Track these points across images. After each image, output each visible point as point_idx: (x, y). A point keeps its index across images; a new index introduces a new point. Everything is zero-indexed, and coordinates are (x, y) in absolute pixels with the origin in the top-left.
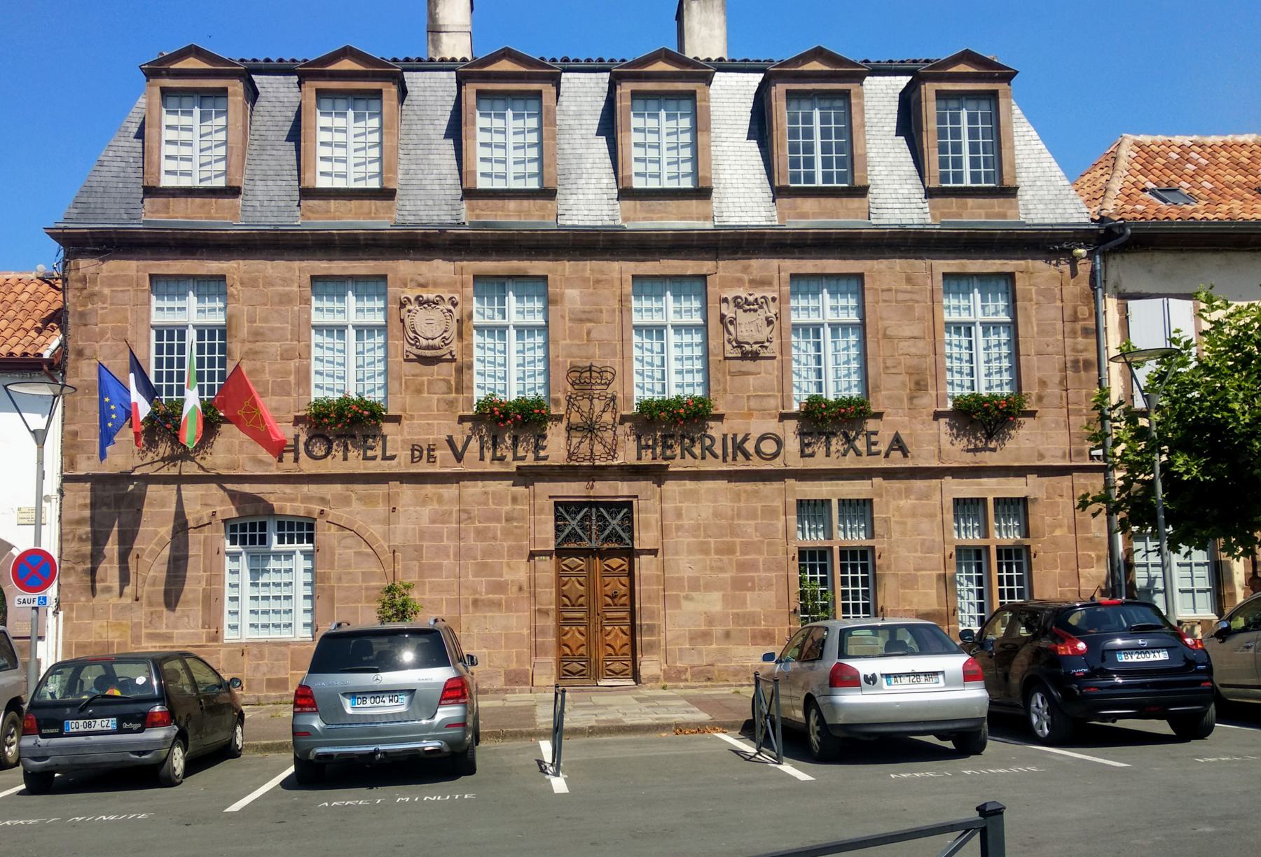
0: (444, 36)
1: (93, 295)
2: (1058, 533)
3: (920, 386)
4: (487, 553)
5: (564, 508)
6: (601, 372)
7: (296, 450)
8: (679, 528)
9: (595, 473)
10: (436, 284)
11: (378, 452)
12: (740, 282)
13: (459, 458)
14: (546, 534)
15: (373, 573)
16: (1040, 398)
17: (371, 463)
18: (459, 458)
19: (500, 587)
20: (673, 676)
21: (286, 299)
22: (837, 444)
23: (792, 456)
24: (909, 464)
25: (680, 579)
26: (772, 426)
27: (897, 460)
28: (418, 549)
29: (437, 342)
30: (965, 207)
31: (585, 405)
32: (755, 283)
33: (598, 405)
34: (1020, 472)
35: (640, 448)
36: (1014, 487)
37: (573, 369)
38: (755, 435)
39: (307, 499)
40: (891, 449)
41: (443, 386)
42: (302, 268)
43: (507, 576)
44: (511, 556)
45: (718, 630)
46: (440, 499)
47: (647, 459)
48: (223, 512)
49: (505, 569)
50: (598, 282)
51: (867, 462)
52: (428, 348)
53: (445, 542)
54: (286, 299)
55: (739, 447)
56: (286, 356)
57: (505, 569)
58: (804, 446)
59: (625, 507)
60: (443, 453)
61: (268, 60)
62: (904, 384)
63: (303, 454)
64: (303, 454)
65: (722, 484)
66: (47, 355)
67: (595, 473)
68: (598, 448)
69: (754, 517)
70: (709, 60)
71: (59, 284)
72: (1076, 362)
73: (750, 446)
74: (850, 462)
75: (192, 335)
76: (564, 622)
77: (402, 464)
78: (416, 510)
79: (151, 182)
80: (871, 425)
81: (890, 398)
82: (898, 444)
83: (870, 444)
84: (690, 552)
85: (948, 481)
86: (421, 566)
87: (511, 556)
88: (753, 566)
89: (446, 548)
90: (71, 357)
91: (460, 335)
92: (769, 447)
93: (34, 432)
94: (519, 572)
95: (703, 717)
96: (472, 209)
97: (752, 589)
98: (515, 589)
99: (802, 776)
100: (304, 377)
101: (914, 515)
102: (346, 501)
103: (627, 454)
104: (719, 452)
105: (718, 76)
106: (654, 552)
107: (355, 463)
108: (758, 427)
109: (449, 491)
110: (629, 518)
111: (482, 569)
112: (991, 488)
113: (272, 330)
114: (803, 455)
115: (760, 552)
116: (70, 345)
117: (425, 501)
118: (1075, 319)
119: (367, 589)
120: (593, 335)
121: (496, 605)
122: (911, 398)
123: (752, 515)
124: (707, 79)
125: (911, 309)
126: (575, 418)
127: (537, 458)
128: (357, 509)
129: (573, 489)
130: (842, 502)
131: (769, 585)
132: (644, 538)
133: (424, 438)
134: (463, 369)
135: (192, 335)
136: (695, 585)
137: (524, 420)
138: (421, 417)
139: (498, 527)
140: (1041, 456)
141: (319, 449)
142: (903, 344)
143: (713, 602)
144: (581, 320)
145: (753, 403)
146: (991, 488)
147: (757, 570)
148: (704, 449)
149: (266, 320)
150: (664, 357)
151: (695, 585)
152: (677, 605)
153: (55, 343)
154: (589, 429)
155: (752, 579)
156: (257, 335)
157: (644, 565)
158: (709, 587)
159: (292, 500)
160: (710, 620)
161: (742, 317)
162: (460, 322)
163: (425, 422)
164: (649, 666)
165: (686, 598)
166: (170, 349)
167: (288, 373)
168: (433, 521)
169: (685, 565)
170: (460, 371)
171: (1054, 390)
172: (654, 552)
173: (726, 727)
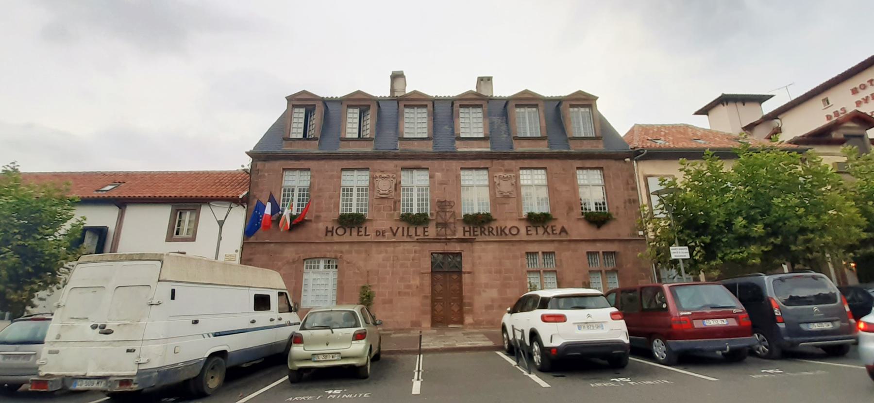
3: (570, 209)
6: (450, 202)
7: (332, 232)
10: (387, 171)
11: (363, 233)
12: (500, 170)
13: (395, 235)
14: (427, 265)
16: (617, 214)
18: (395, 235)
19: (409, 287)
20: (477, 324)
21: (331, 177)
22: (541, 230)
24: (568, 238)
26: (516, 224)
27: (564, 237)
28: (378, 272)
31: (442, 214)
32: (507, 171)
34: (612, 241)
35: (465, 231)
37: (439, 201)
38: (509, 227)
39: (336, 251)
43: (412, 282)
46: (386, 252)
47: (467, 236)
51: (552, 237)
54: (331, 177)
55: (502, 231)
56: (331, 198)
58: (527, 231)
59: (459, 254)
66: (241, 197)
71: (435, 255)
73: (507, 231)
74: (545, 237)
75: (296, 193)
76: (434, 301)
77: (372, 237)
78: (378, 257)
79: (286, 136)
80: (552, 223)
82: (563, 230)
83: (553, 230)
91: (396, 189)
92: (514, 232)
93: (218, 222)
94: (416, 281)
95: (490, 343)
96: (401, 144)
99: (544, 384)
100: (337, 205)
102: (350, 252)
103: (459, 235)
104: (495, 233)
106: (469, 273)
107: (355, 237)
108: (509, 224)
109: (390, 249)
111: (402, 279)
112: (601, 248)
116: (251, 193)
117: (380, 253)
118: (628, 184)
126: (440, 220)
127: (424, 235)
128: (356, 257)
129: (438, 248)
130: (543, 253)
132: (466, 267)
133: (382, 228)
134: (396, 202)
135: (296, 193)
136: (487, 286)
137: (420, 220)
140: (619, 235)
141: (340, 231)
143: (494, 293)
146: (601, 248)
148: (489, 232)
150: (475, 192)
151: (487, 286)
152: (480, 294)
153: (245, 193)
154: (444, 225)
156: (320, 190)
157: (466, 278)
160: (493, 300)
161: (502, 183)
162: (396, 185)
163: (382, 222)
164: (468, 319)
169: (483, 278)
170: (395, 202)
171: (622, 211)
172: (469, 273)
173: (501, 348)
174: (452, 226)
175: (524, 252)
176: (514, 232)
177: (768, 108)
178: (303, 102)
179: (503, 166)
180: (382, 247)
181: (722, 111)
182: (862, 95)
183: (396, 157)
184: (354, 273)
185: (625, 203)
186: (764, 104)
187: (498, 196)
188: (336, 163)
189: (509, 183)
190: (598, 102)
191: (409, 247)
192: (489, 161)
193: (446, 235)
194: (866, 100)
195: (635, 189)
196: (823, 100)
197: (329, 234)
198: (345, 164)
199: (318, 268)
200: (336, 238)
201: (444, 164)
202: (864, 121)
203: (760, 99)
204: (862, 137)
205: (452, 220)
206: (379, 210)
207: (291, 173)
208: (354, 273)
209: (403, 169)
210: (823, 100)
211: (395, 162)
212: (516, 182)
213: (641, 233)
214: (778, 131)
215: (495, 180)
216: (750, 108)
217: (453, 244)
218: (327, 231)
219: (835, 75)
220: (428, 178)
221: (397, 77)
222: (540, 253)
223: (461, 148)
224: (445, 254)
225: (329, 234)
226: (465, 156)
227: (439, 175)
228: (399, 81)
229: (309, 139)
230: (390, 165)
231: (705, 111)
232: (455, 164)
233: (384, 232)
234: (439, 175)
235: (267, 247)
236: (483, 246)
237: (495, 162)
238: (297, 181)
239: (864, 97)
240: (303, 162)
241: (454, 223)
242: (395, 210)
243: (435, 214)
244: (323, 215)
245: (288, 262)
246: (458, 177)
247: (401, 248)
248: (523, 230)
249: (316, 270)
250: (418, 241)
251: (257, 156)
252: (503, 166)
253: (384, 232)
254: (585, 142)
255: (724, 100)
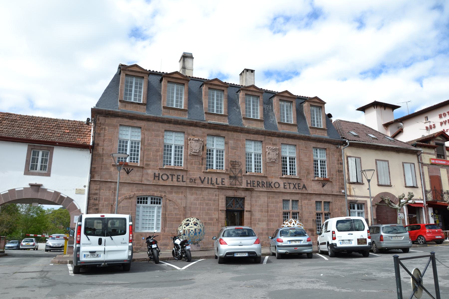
0: (187, 70)
1: (102, 128)
2: (336, 210)
4: (209, 209)
5: (228, 199)
7: (159, 177)
8: (256, 205)
9: (237, 189)
10: (197, 136)
11: (181, 180)
12: (270, 144)
13: (202, 182)
14: (222, 205)
15: (178, 214)
17: (179, 183)
18: (202, 182)
19: (211, 219)
23: (282, 189)
25: (256, 219)
29: (197, 151)
30: (316, 132)
33: (237, 171)
35: (247, 183)
36: (328, 199)
37: (231, 161)
38: (274, 182)
40: (303, 187)
41: (198, 163)
42: (313, 144)
44: (214, 211)
45: (265, 232)
46: (196, 194)
48: (137, 194)
49: (213, 214)
50: (237, 140)
52: (195, 152)
53: (197, 206)
55: (270, 185)
57: (213, 214)
58: (284, 186)
59: (243, 199)
60: (198, 181)
61: (150, 70)
62: (305, 173)
63: (160, 179)
64: (160, 179)
65: (266, 193)
67: (237, 189)
68: (237, 183)
69: (273, 203)
70: (163, 73)
72: (339, 170)
73: (272, 185)
81: (302, 175)
82: (304, 187)
83: (299, 186)
84: (258, 212)
85: (314, 197)
86: (191, 213)
87: (214, 211)
88: (273, 216)
89: (197, 207)
90: (95, 146)
92: (277, 186)
94: (215, 216)
97: (272, 222)
98: (215, 220)
101: (308, 205)
102: (171, 193)
103: (244, 186)
104: (266, 186)
105: (191, 81)
108: (274, 180)
110: (244, 202)
111: (207, 214)
112: (323, 199)
113: (153, 143)
114: (284, 188)
115: (274, 212)
119: (176, 218)
120: (236, 153)
121: (210, 224)
122: (307, 176)
123: (273, 203)
124: (188, 81)
125: (306, 154)
127: (222, 184)
129: (231, 194)
131: (276, 221)
132: (247, 207)
136: (260, 220)
138: (192, 171)
139: (212, 202)
142: (305, 163)
144: (233, 149)
145: (273, 174)
147: (274, 217)
148: (262, 185)
149: (151, 140)
151: (260, 220)
155: (272, 219)
158: (262, 221)
159: (157, 192)
162: (203, 147)
165: (257, 224)
166: (220, 155)
167: (157, 156)
168: (194, 200)
169: (257, 215)
174: (240, 179)
175: (282, 199)
176: (277, 186)
177: (397, 114)
178: (129, 72)
179: (271, 141)
180: (194, 191)
181: (373, 113)
182: (444, 119)
183: (205, 126)
184: (174, 208)
185: (336, 172)
186: (395, 110)
187: (268, 161)
188: (161, 125)
189: (275, 153)
190: (325, 105)
191: (211, 191)
192: (263, 136)
193: (236, 185)
194: (445, 122)
195: (341, 164)
196: (426, 117)
197: (157, 178)
198: (167, 126)
199: (146, 203)
200: (161, 182)
201: (236, 135)
202: (443, 135)
203: (393, 107)
204: (443, 145)
205: (239, 175)
206: (192, 164)
207: (171, 134)
208: (174, 208)
209: (208, 135)
210: (426, 117)
211: (203, 129)
212: (279, 153)
213: (343, 191)
214: (400, 132)
215: (267, 150)
216: (388, 111)
217: (240, 191)
218: (155, 176)
219: (433, 105)
220: (224, 143)
221: (186, 57)
222: (291, 201)
223: (246, 125)
224: (235, 198)
225: (157, 178)
226: (248, 131)
227: (231, 142)
228: (188, 61)
229: (403, 166)
230: (199, 131)
231: (363, 109)
232: (242, 136)
233: (195, 180)
234: (231, 142)
235: (109, 185)
236: (259, 194)
237: (267, 137)
238: (130, 135)
239: (445, 120)
240: (135, 121)
241: (241, 177)
242: (202, 165)
243: (229, 170)
244: (152, 163)
245: (126, 198)
246: (244, 145)
247: (205, 193)
248: (282, 185)
249: (145, 205)
250: (219, 188)
251: (95, 112)
252: (271, 141)
253: (195, 180)
254: (318, 131)
255: (376, 104)
